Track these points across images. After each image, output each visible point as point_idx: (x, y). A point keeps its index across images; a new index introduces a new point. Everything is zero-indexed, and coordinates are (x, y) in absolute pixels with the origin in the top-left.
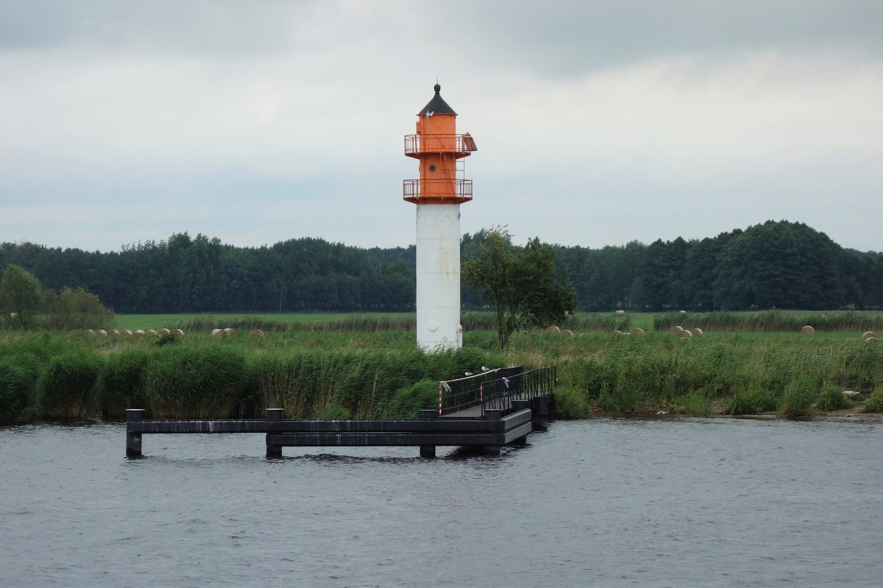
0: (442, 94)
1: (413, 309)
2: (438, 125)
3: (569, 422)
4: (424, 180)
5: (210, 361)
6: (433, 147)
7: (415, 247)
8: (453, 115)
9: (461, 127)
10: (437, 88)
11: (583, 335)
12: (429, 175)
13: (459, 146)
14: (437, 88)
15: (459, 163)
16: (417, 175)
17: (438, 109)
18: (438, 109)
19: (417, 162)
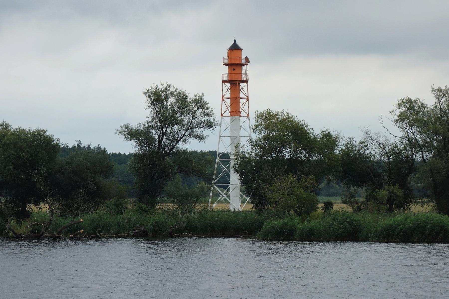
0: (237, 42)
1: (215, 152)
2: (235, 53)
3: (281, 247)
4: (230, 74)
5: (348, 223)
6: (234, 61)
7: (247, 57)
8: (241, 50)
9: (244, 55)
10: (235, 41)
11: (304, 186)
12: (233, 72)
13: (244, 61)
14: (235, 41)
15: (243, 67)
16: (227, 72)
17: (235, 48)
18: (235, 48)
19: (227, 67)
